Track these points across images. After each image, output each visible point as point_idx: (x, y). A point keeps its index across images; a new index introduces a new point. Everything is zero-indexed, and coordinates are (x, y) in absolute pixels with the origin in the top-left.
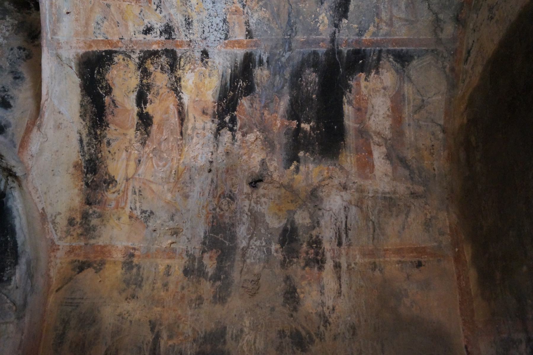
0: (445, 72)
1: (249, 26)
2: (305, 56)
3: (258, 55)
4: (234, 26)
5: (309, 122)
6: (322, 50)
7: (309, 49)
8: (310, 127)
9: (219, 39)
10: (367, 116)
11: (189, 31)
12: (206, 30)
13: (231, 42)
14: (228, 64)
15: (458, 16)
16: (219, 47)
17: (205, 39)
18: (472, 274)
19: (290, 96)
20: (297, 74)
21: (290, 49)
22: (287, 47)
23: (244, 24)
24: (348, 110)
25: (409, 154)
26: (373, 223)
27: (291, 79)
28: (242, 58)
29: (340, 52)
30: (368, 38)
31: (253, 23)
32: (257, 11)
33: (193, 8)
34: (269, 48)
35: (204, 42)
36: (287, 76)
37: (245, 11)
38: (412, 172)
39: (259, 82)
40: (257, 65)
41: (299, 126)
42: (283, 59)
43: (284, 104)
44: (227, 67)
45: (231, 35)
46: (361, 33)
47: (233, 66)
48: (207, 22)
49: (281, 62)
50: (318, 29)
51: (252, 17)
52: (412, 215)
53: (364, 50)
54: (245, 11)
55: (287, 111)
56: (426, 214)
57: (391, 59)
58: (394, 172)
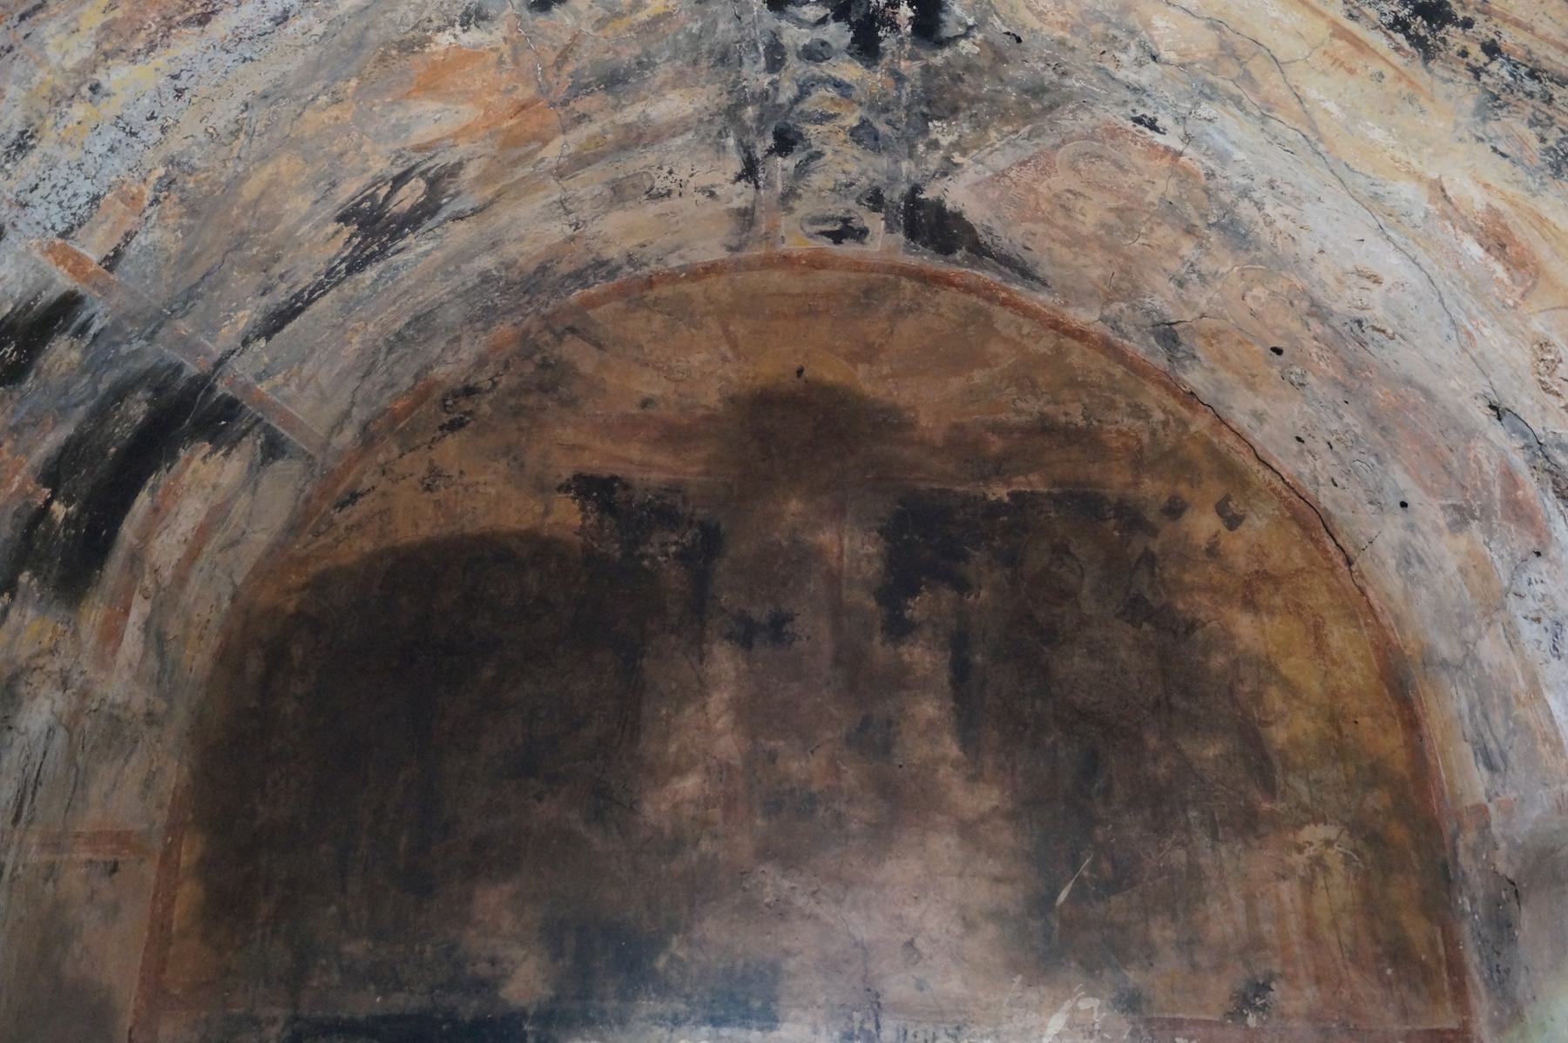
0: (298, 498)
1: (127, 243)
2: (162, 365)
3: (91, 311)
4: (102, 222)
5: (68, 501)
6: (192, 369)
7: (175, 356)
8: (66, 514)
9: (49, 226)
10: (158, 529)
11: (7, 162)
12: (44, 189)
13: (65, 248)
14: (19, 291)
15: (368, 423)
16: (34, 242)
17: (24, 205)
18: (189, 893)
19: (76, 430)
20: (120, 393)
21: (151, 338)
22: (149, 330)
23: (122, 234)
24: (143, 501)
25: (174, 628)
26: (78, 770)
27: (104, 398)
28: (57, 296)
29: (212, 389)
30: (264, 390)
31: (138, 244)
32: (166, 227)
33: (61, 125)
34: (122, 312)
35: (15, 211)
36: (103, 387)
37: (148, 212)
38: (162, 670)
39: (45, 367)
40: (70, 332)
41: (48, 503)
42: (124, 349)
43: (51, 440)
44: (12, 296)
45: (79, 237)
46: (259, 378)
47: (25, 301)
48: (59, 176)
49: (118, 351)
50: (220, 329)
51: (147, 233)
52: (134, 761)
53: (243, 407)
54: (148, 212)
55: (48, 459)
56: (152, 761)
57: (259, 442)
58: (142, 662)
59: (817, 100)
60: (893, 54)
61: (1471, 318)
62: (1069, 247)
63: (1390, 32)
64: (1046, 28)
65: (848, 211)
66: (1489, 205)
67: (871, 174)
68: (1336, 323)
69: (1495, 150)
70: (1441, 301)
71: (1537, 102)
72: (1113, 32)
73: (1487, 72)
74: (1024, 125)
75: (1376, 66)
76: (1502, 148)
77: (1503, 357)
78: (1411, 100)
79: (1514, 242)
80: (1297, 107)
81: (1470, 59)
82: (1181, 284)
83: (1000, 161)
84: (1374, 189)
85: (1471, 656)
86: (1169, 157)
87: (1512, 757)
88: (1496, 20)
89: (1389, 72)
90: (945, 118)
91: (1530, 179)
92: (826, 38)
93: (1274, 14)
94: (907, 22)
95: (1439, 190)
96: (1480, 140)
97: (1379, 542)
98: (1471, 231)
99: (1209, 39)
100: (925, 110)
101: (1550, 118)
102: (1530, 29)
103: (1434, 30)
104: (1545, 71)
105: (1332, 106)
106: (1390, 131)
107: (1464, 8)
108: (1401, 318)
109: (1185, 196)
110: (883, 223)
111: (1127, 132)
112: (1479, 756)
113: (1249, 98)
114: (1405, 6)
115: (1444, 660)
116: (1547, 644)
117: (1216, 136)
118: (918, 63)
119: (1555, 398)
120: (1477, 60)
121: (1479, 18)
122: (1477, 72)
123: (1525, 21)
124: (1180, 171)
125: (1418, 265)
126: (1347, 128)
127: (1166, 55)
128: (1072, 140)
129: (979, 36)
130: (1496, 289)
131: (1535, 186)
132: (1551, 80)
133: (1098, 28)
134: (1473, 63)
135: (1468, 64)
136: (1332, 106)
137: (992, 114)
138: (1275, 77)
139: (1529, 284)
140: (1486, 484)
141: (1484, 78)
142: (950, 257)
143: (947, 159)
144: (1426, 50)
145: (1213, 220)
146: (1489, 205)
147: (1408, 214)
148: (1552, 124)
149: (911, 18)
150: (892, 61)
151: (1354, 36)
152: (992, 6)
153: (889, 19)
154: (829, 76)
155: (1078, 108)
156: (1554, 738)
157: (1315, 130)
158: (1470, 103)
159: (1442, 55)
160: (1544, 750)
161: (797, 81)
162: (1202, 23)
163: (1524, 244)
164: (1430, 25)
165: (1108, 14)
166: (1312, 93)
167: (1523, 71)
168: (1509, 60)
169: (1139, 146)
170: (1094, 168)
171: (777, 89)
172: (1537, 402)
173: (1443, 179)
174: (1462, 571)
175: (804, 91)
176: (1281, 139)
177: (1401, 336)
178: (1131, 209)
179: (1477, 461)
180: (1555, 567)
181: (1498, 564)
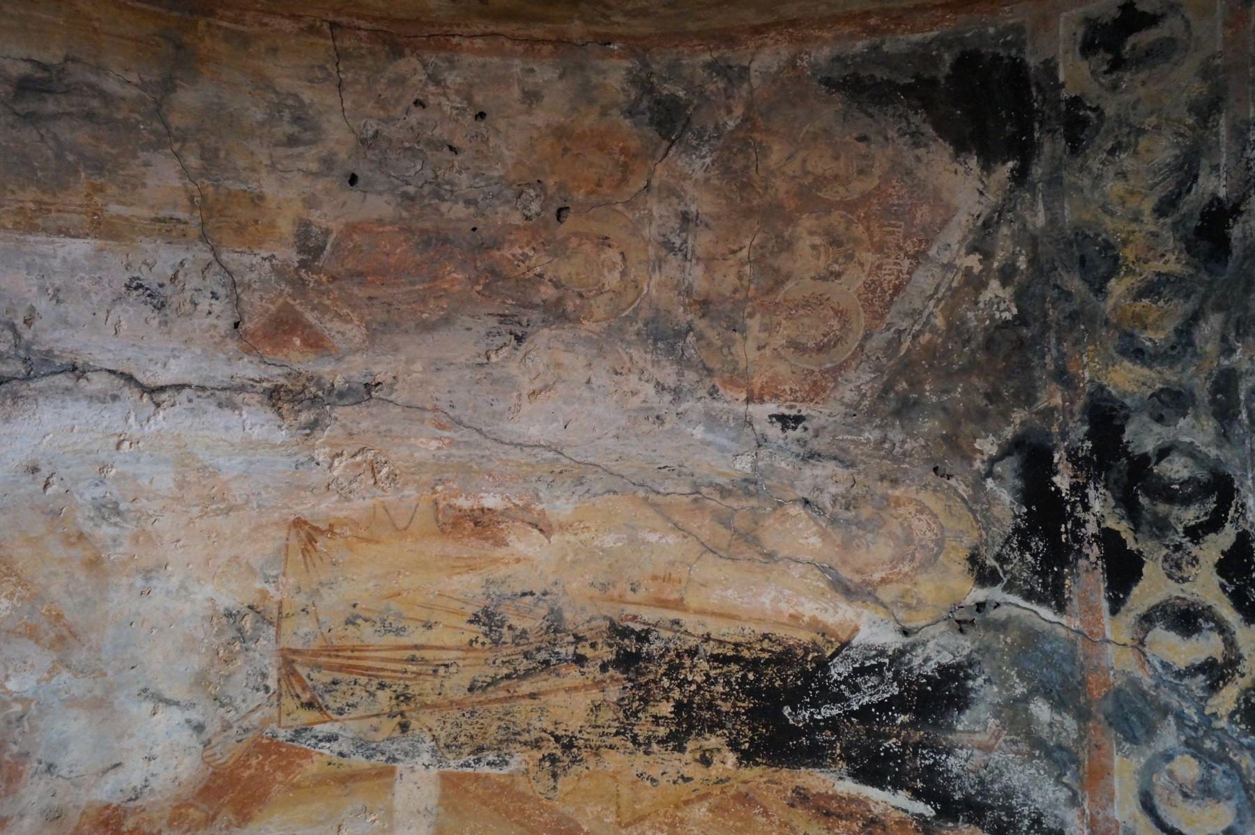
59: (1166, 322)
60: (1072, 414)
61: (453, 443)
62: (817, 178)
63: (646, 627)
64: (913, 495)
65: (1115, 87)
66: (507, 545)
67: (1086, 182)
68: (536, 316)
69: (532, 594)
70: (479, 431)
71: (531, 648)
72: (851, 514)
73: (572, 643)
74: (909, 350)
75: (642, 594)
76: (528, 599)
77: (409, 438)
78: (604, 587)
79: (473, 534)
80: (676, 518)
81: (587, 644)
82: (685, 218)
83: (924, 279)
84: (585, 488)
85: (166, 139)
86: (756, 392)
87: (28, 135)
88: (589, 682)
89: (630, 596)
90: (998, 328)
91: (498, 593)
92: (1157, 428)
93: (730, 592)
94: (1060, 467)
95: (544, 528)
96: (545, 594)
97: (332, 99)
98: (502, 514)
99: (770, 540)
100: (1024, 331)
101: (518, 645)
102: (568, 690)
103: (620, 648)
104: (542, 671)
105: (653, 538)
106: (602, 551)
107: (612, 677)
108: (495, 382)
109: (725, 351)
110: (1062, 78)
111: (803, 401)
112: (40, 74)
113: (715, 502)
114: (647, 653)
115: (174, 89)
116: (149, 279)
117: (725, 442)
118: (1041, 405)
119: (353, 453)
120: (583, 646)
121: (599, 677)
122: (578, 639)
123: (574, 694)
124: (742, 382)
125: (516, 445)
126: (633, 528)
127: (796, 510)
128: (854, 355)
129: (978, 464)
130: (455, 486)
131: (493, 589)
132: (534, 668)
133: (866, 512)
134: (584, 643)
135: (586, 640)
136: (653, 538)
137: (946, 354)
138: (705, 535)
139: (440, 517)
140: (325, 310)
141: (571, 639)
142: (957, 50)
143: (987, 256)
144: (618, 631)
145: (691, 338)
146: (507, 545)
147: (550, 485)
148: (513, 642)
149: (1056, 473)
150: (1072, 403)
151: (667, 607)
152: (971, 509)
153: (1081, 468)
154: (1150, 368)
155: (859, 403)
156: (39, 221)
157: (654, 505)
158: (568, 615)
159: (605, 635)
160: (29, 196)
161: (1195, 354)
162: (780, 556)
163: (466, 540)
164: (625, 651)
165: (861, 532)
166: (672, 539)
167: (554, 661)
168: (566, 661)
169: (787, 388)
170: (823, 329)
171: (1224, 339)
172: (359, 433)
173: (546, 541)
174: (257, 199)
175: (1185, 333)
176: (674, 475)
177: (481, 365)
178: (770, 291)
179: (346, 319)
180: (217, 339)
181: (246, 259)
